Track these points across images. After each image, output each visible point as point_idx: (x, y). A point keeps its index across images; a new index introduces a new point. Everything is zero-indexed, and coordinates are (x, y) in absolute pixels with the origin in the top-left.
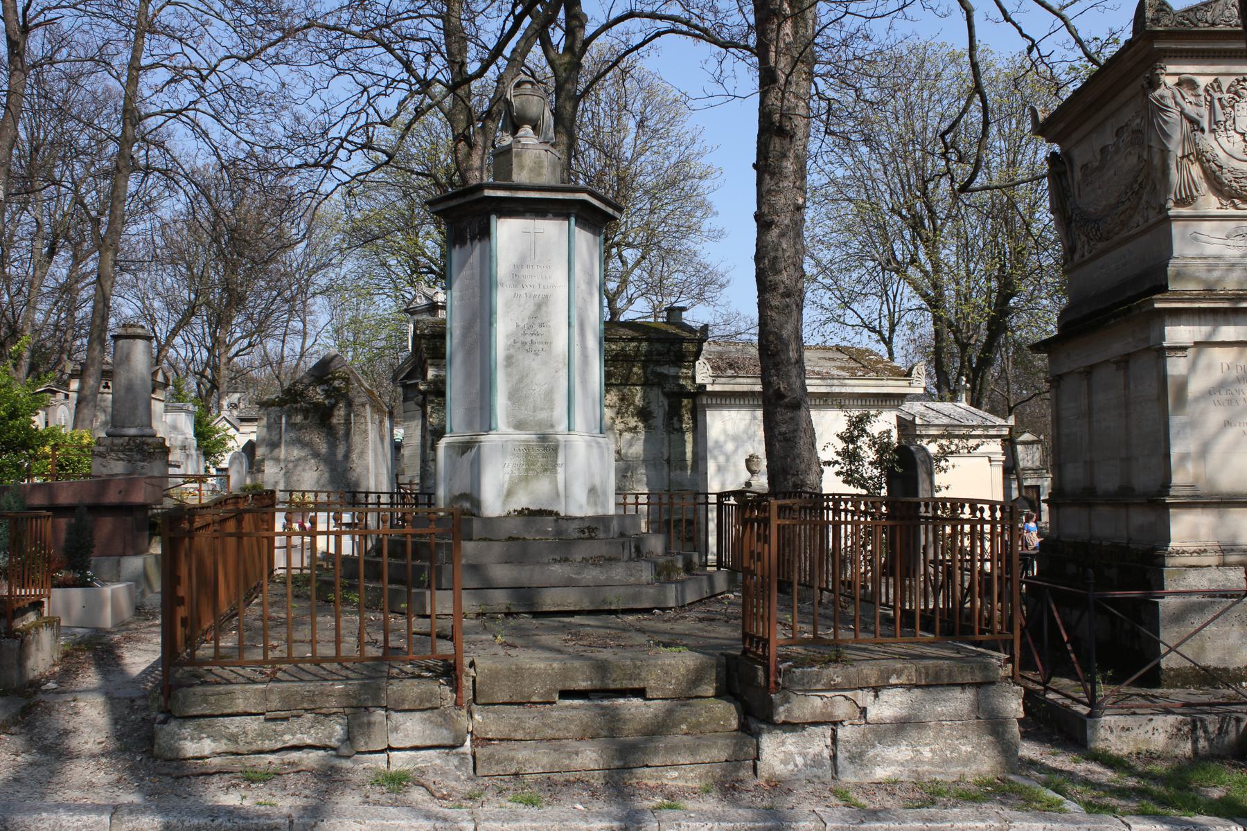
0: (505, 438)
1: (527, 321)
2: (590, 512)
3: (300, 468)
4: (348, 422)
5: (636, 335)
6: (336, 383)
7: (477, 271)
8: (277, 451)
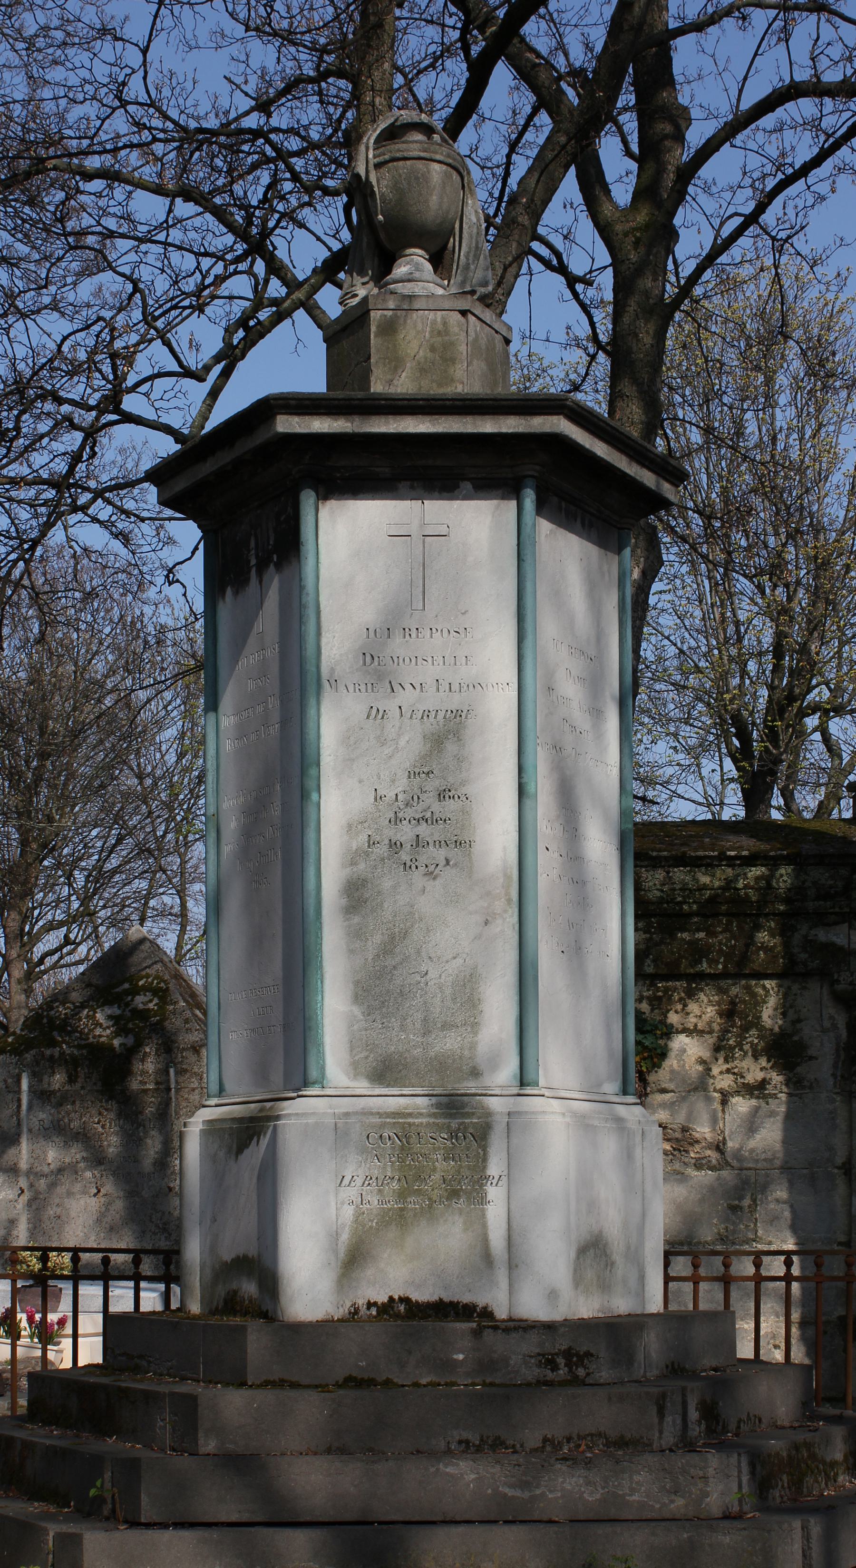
0: (345, 1105)
1: (402, 783)
2: (586, 1308)
3: (61, 1190)
4: (163, 1087)
5: (763, 846)
6: (140, 1001)
7: (272, 653)
8: (12, 1151)
